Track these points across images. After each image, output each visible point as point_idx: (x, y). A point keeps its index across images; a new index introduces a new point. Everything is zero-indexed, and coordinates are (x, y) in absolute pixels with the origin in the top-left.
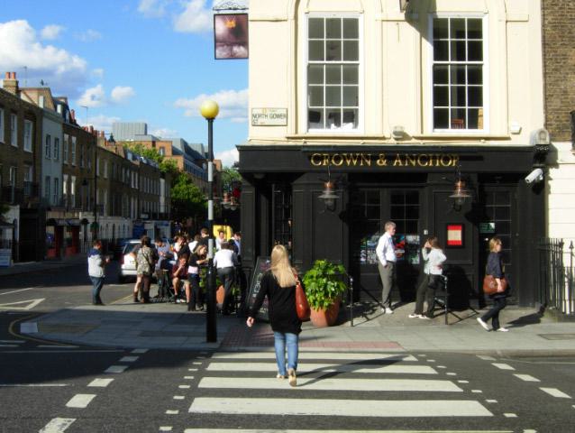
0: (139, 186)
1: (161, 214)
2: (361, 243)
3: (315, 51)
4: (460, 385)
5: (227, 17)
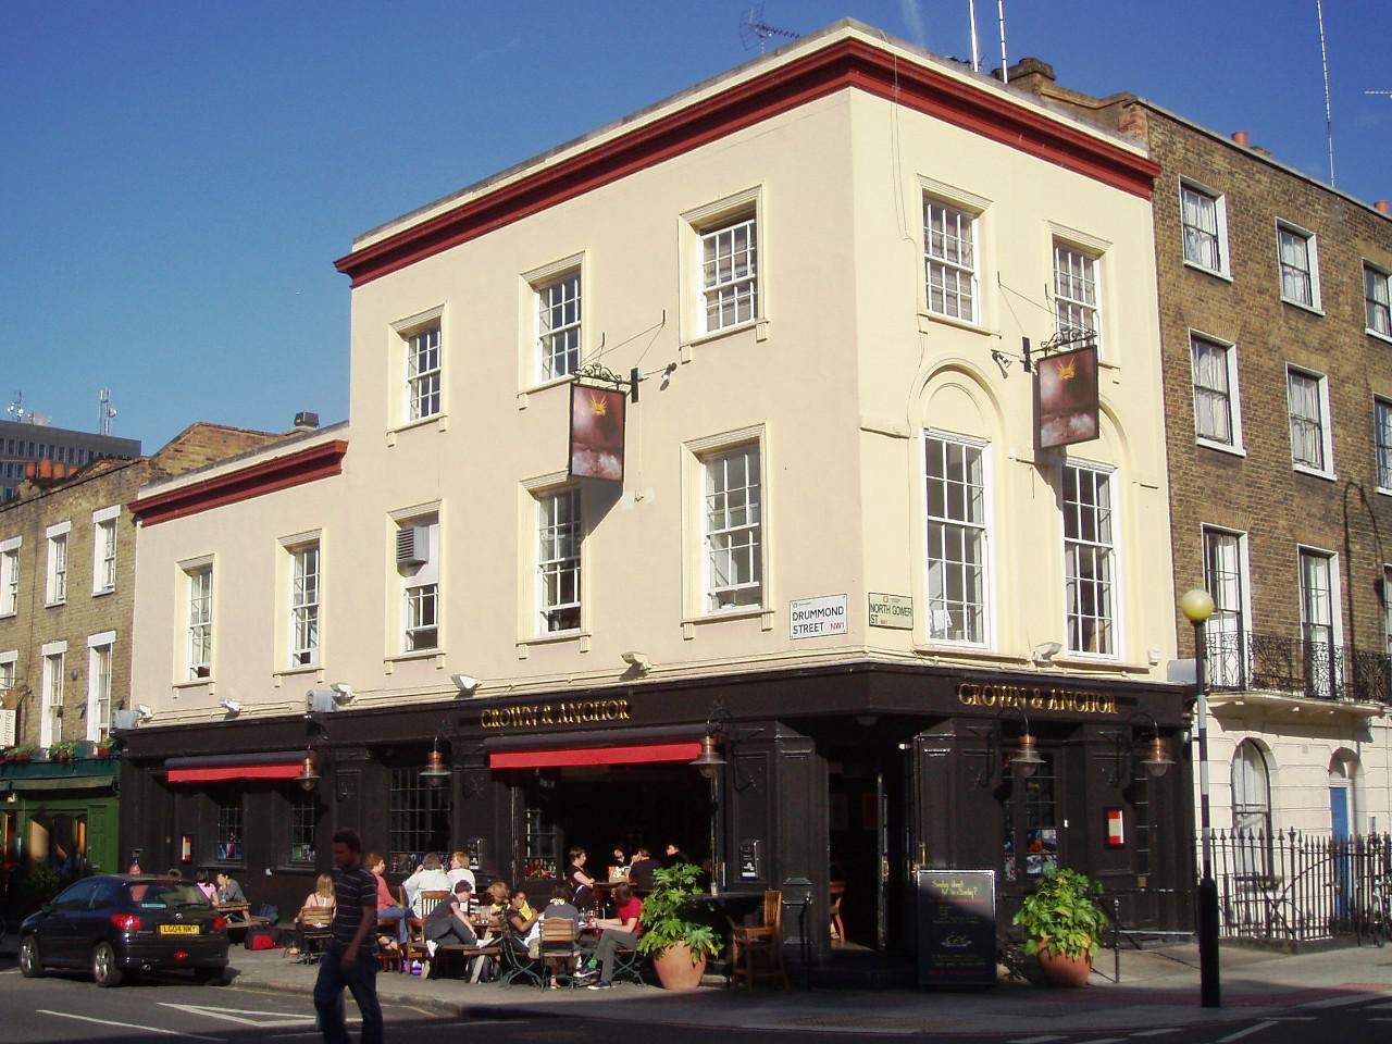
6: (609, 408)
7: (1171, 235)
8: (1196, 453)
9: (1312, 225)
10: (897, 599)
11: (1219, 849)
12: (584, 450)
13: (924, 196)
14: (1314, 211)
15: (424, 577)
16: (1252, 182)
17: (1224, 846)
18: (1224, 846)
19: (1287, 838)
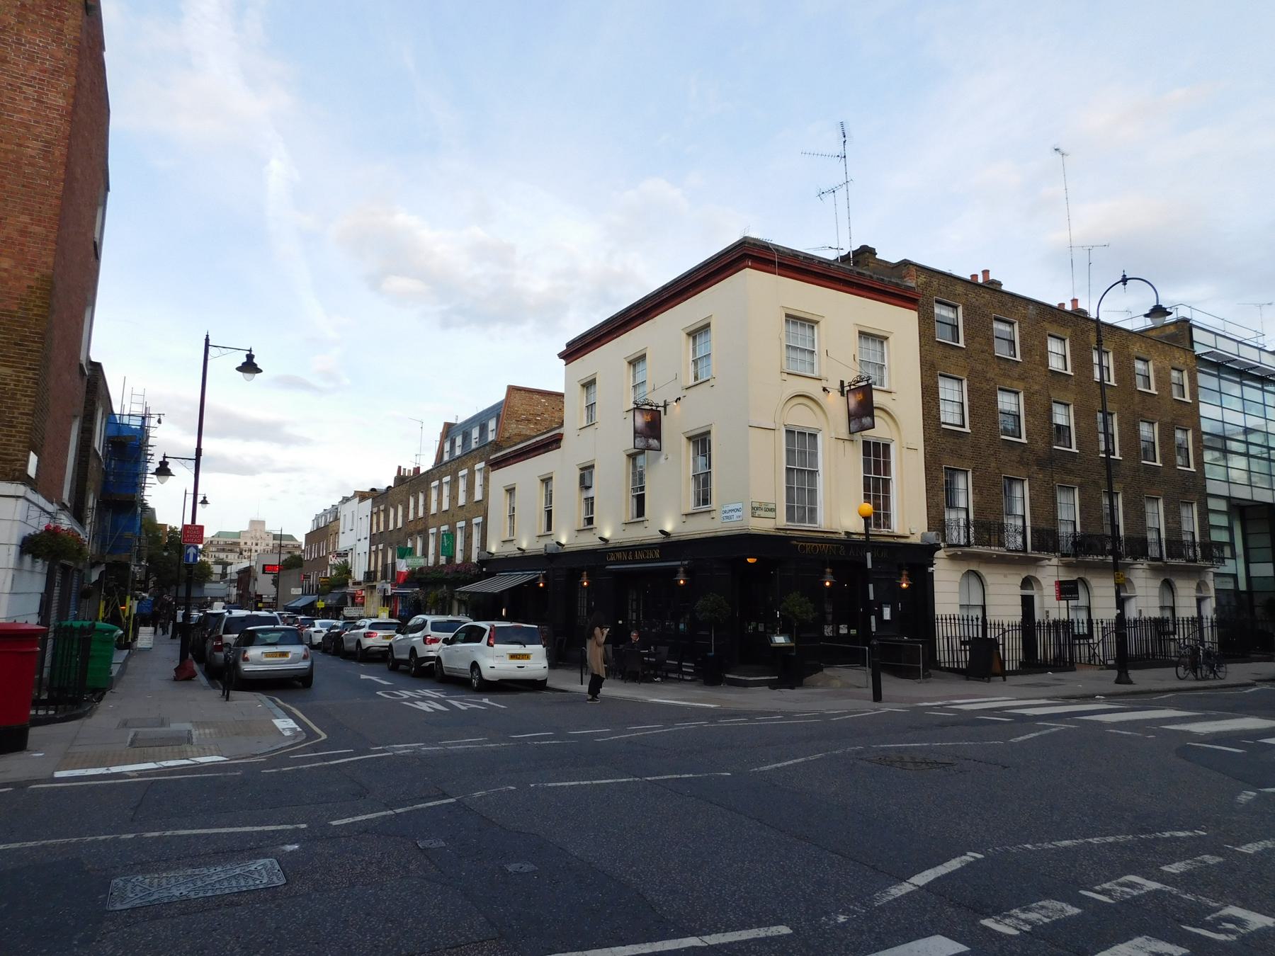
6: (864, 395)
7: (927, 324)
8: (941, 432)
9: (1016, 317)
10: (767, 504)
11: (940, 624)
12: (641, 437)
13: (786, 316)
14: (1017, 310)
15: (591, 493)
16: (978, 298)
17: (946, 623)
18: (946, 623)
19: (975, 620)
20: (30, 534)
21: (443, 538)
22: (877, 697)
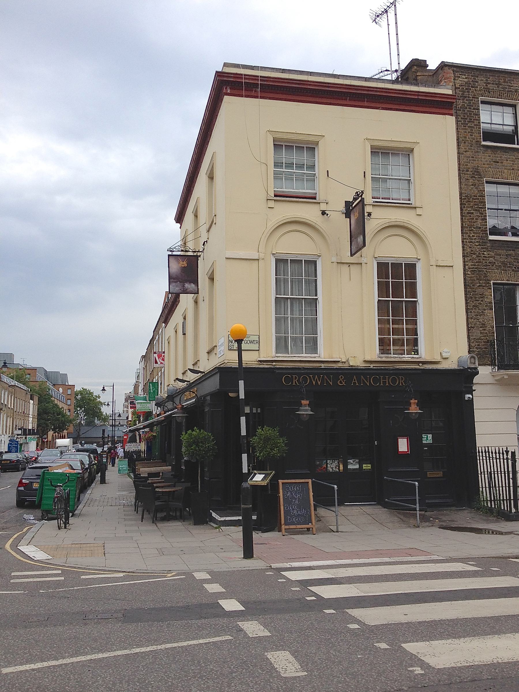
0: (14, 407)
1: (29, 430)
2: (348, 462)
3: (383, 289)
4: (284, 577)
5: (179, 258)
20: (91, 393)
21: (150, 386)
22: (248, 553)
